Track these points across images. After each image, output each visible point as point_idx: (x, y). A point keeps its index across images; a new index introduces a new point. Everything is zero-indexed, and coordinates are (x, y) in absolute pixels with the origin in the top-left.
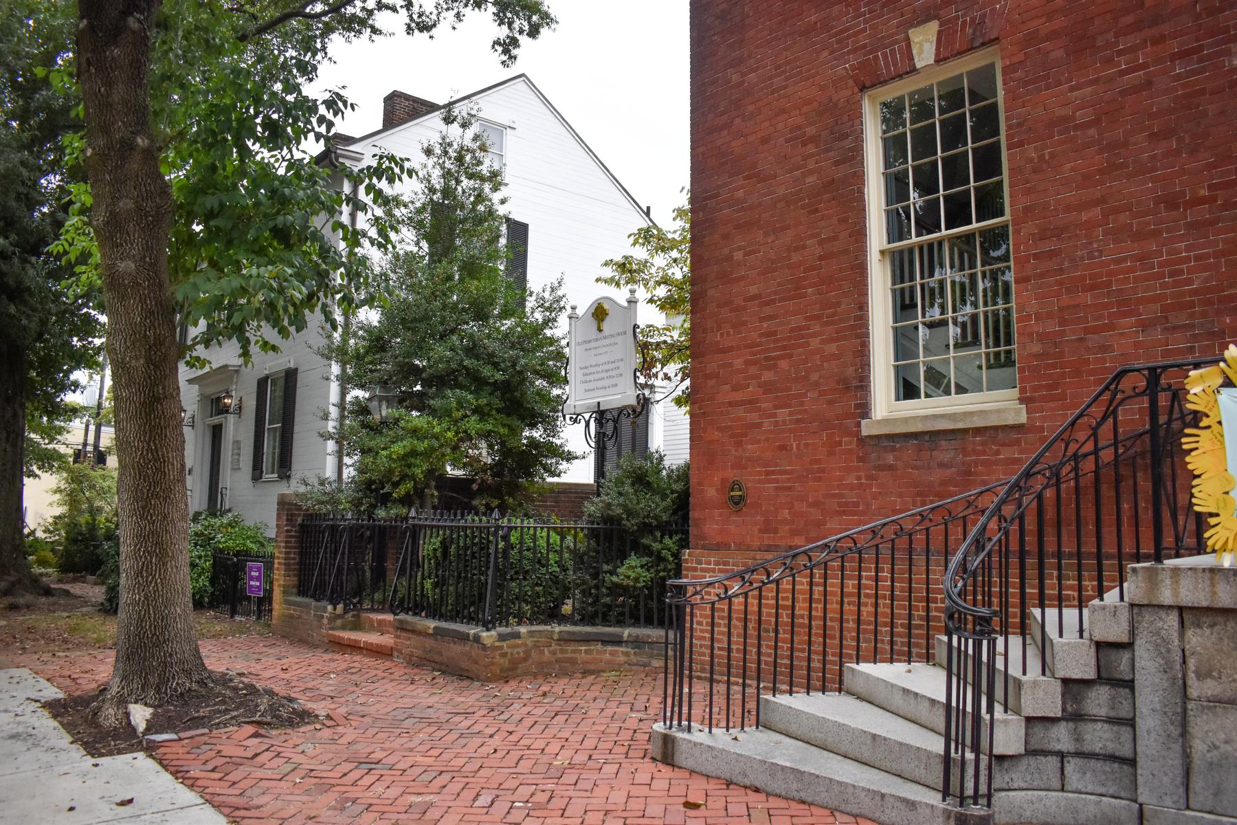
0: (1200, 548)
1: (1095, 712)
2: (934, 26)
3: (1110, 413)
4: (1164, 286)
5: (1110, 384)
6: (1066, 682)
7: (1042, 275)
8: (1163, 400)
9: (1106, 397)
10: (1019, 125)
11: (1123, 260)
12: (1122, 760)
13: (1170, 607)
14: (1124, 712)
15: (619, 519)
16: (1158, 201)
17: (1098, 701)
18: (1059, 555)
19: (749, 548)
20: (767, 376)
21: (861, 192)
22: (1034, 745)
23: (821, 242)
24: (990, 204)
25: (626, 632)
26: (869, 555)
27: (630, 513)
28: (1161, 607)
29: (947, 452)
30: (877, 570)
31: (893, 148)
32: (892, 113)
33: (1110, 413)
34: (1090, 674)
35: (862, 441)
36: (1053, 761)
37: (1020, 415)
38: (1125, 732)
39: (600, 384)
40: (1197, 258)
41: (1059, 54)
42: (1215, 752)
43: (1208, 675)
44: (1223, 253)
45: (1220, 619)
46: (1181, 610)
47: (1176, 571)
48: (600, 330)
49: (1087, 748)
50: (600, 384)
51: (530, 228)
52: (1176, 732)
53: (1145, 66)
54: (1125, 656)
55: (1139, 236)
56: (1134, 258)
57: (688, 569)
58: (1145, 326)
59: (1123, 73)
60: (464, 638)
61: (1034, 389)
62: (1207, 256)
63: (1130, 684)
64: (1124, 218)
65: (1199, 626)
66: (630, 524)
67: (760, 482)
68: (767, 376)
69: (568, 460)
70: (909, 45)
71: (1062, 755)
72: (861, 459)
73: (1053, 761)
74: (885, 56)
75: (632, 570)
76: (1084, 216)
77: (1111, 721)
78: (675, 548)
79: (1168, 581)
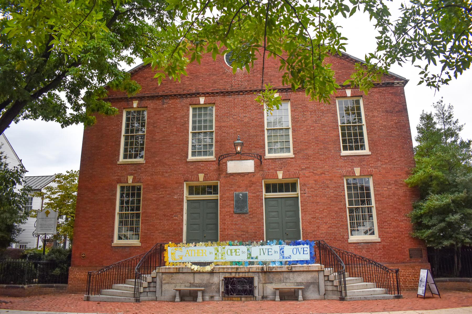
0: (164, 265)
2: (132, 177)
6: (148, 282)
7: (145, 223)
8: (162, 248)
12: (154, 292)
14: (155, 286)
15: (55, 261)
16: (163, 215)
17: (152, 285)
19: (85, 266)
20: (93, 233)
21: (115, 202)
23: (107, 209)
24: (138, 209)
25: (55, 285)
26: (117, 267)
27: (58, 259)
29: (127, 250)
32: (122, 188)
35: (112, 247)
36: (146, 293)
37: (139, 244)
38: (155, 288)
44: (171, 224)
46: (162, 273)
48: (47, 216)
49: (150, 291)
53: (163, 194)
54: (155, 279)
55: (160, 220)
57: (70, 271)
58: (160, 233)
59: (160, 194)
60: (19, 287)
63: (156, 282)
66: (57, 261)
67: (89, 253)
68: (93, 233)
70: (127, 178)
73: (146, 293)
74: (123, 179)
75: (57, 271)
77: (153, 287)
78: (66, 266)
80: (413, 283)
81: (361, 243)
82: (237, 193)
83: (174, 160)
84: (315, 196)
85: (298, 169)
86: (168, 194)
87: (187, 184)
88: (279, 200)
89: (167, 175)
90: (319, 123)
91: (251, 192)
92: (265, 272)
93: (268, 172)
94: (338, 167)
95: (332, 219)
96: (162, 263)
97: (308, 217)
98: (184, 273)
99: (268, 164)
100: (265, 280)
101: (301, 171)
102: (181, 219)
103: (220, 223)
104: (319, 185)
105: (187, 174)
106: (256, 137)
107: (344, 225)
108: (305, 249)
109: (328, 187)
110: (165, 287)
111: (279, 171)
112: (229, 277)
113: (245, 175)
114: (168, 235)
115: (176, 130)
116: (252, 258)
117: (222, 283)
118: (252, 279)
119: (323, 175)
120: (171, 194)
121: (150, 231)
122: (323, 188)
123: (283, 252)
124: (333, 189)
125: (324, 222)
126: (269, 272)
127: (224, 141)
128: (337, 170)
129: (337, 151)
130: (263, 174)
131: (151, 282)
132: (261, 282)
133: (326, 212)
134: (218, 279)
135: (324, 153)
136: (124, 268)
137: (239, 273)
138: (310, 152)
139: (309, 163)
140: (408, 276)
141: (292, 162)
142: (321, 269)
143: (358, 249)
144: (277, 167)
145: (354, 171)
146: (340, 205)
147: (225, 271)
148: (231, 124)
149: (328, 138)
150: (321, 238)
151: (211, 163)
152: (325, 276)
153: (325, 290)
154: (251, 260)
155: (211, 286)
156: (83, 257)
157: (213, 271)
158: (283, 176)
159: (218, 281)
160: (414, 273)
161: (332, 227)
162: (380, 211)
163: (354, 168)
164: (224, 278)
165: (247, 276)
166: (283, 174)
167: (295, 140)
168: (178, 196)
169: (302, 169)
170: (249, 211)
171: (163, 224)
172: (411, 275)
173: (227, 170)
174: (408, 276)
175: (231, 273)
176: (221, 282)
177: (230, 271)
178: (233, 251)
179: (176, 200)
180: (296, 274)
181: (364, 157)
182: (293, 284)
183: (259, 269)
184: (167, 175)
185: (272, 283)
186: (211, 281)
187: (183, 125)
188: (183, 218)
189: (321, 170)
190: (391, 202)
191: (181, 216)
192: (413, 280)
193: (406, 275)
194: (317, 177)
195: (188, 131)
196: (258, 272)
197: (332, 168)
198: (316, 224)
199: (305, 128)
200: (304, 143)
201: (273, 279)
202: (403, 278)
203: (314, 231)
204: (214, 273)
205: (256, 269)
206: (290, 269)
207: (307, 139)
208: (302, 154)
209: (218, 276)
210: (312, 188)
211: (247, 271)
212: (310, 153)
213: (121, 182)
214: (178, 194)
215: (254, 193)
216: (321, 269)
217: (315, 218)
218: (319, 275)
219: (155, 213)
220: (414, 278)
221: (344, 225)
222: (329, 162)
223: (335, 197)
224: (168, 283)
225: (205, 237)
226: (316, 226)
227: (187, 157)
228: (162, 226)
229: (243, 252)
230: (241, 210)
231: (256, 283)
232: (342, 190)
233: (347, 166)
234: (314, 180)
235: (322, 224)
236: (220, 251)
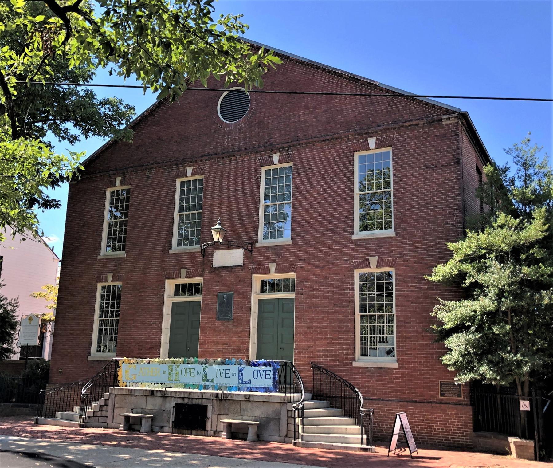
17: (104, 408)
20: (71, 344)
22: (95, 415)
31: (182, 192)
34: (103, 404)
39: (29, 338)
50: (29, 338)
51: (4, 260)
53: (143, 296)
63: (108, 405)
68: (71, 344)
69: (14, 354)
71: (99, 417)
72: (87, 365)
80: (451, 435)
81: (370, 367)
93: (259, 265)
96: (115, 382)
98: (137, 395)
100: (220, 410)
101: (298, 262)
108: (268, 372)
109: (332, 285)
116: (208, 381)
117: (173, 410)
118: (206, 407)
119: (326, 268)
123: (242, 375)
126: (225, 400)
130: (253, 267)
131: (103, 405)
138: (311, 235)
140: (435, 423)
142: (284, 400)
143: (366, 376)
147: (178, 396)
150: (318, 357)
154: (207, 383)
156: (60, 372)
157: (165, 394)
160: (445, 419)
161: (333, 343)
162: (402, 321)
164: (176, 404)
165: (190, 403)
166: (276, 267)
169: (300, 260)
172: (440, 421)
174: (435, 423)
175: (183, 398)
176: (172, 409)
177: (182, 396)
178: (188, 370)
180: (255, 404)
186: (163, 408)
188: (161, 326)
190: (419, 308)
191: (160, 323)
192: (442, 429)
193: (431, 421)
194: (318, 271)
201: (228, 409)
202: (427, 426)
203: (309, 347)
210: (311, 286)
211: (200, 397)
213: (100, 282)
216: (284, 400)
217: (312, 328)
220: (444, 427)
227: (170, 247)
229: (198, 373)
231: (209, 414)
236: (174, 370)
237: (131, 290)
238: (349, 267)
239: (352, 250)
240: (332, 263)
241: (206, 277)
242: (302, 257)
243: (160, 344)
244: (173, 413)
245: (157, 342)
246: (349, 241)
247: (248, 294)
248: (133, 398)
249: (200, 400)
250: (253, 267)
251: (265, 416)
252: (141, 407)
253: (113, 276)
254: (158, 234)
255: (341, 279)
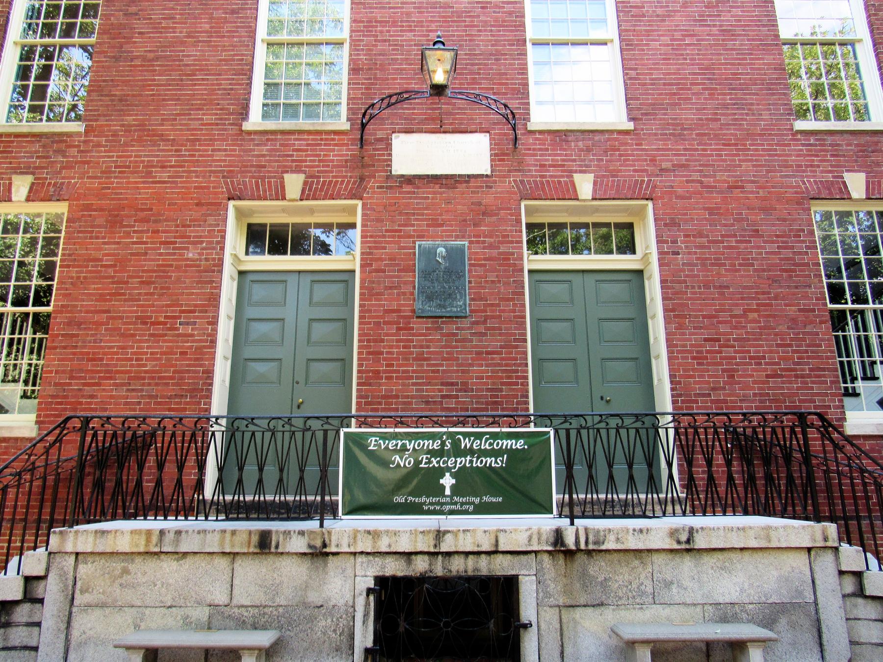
1: (19, 620)
2: (29, 179)
3: (59, 440)
4: (132, 365)
5: (61, 424)
7: (65, 348)
9: (57, 432)
10: (70, 255)
11: (112, 347)
13: (72, 553)
18: (855, 498)
28: (66, 553)
30: (11, 535)
33: (59, 440)
34: (19, 596)
40: (152, 353)
41: (101, 221)
42: (84, 636)
43: (87, 591)
45: (97, 559)
47: (77, 532)
52: (63, 626)
53: (146, 243)
56: (119, 347)
61: (46, 416)
62: (157, 353)
63: (41, 601)
64: (119, 324)
65: (86, 563)
76: (96, 318)
79: (72, 538)
82: (426, 243)
83: (195, 124)
84: (712, 264)
85: (646, 171)
86: (162, 243)
87: (240, 213)
88: (577, 279)
89: (165, 176)
90: (714, 26)
91: (478, 242)
92: (569, 554)
93: (542, 177)
94: (786, 166)
95: (778, 345)
97: (693, 338)
98: (185, 554)
99: (540, 150)
100: (567, 591)
102: (209, 335)
103: (359, 353)
104: (725, 225)
105: (241, 172)
106: (496, 60)
107: (824, 370)
109: (756, 233)
110: (83, 623)
111: (581, 172)
112: (400, 574)
113: (460, 182)
114: (150, 397)
115: (207, 27)
117: (367, 604)
118: (510, 584)
120: (175, 243)
121: (80, 378)
122: (741, 236)
124: (778, 242)
125: (751, 358)
126: (589, 553)
127: (382, 68)
128: (786, 176)
129: (781, 115)
132: (552, 601)
133: (754, 321)
134: (348, 585)
135: (736, 120)
136: (19, 526)
137: (449, 554)
139: (685, 150)
141: (626, 144)
142: (826, 539)
144: (574, 160)
145: (844, 183)
146: (805, 297)
148: (408, 14)
149: (747, 74)
151: (333, 140)
152: (841, 573)
153: (852, 643)
155: (312, 619)
157: (325, 545)
158: (595, 191)
159: (348, 597)
161: (781, 376)
163: (845, 175)
166: (595, 183)
167: (633, 73)
168: (203, 249)
169: (661, 170)
170: (471, 311)
171: (133, 353)
173: (390, 166)
175: (408, 555)
176: (361, 601)
179: (192, 264)
180: (709, 560)
181: (876, 139)
182: (699, 609)
183: (544, 537)
184: (165, 176)
185: (602, 604)
186: (314, 598)
187: (233, 12)
188: (215, 330)
189: (729, 176)
191: (209, 323)
195: (252, 33)
196: (536, 552)
197: (768, 172)
198: (721, 364)
199: (666, 40)
200: (665, 84)
204: (327, 554)
205: (530, 538)
206: (684, 537)
207: (674, 74)
208: (661, 119)
209: (350, 572)
210: (701, 235)
211: (486, 547)
212: (686, 119)
214: (202, 242)
215: (491, 246)
216: (826, 539)
218: (816, 569)
219: (108, 311)
221: (824, 370)
222: (757, 150)
223: (786, 271)
224: (103, 605)
225: (299, 407)
226: (723, 371)
227: (244, 112)
228: (131, 359)
230: (440, 306)
231: (528, 610)
232: (807, 247)
233: (818, 166)
234: (705, 209)
235: (745, 364)
237: (99, 226)
238: (796, 193)
239: (798, 156)
240: (753, 182)
241: (370, 198)
242: (665, 165)
243: (211, 384)
244: (366, 615)
245: (201, 378)
246: (787, 135)
247: (513, 248)
248: (168, 566)
249: (483, 561)
250: (522, 182)
251: (756, 599)
252: (209, 599)
253: (33, 184)
254: (203, 80)
255: (778, 219)
